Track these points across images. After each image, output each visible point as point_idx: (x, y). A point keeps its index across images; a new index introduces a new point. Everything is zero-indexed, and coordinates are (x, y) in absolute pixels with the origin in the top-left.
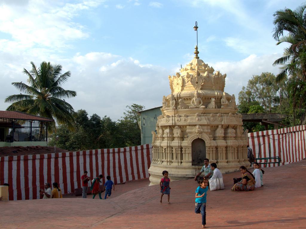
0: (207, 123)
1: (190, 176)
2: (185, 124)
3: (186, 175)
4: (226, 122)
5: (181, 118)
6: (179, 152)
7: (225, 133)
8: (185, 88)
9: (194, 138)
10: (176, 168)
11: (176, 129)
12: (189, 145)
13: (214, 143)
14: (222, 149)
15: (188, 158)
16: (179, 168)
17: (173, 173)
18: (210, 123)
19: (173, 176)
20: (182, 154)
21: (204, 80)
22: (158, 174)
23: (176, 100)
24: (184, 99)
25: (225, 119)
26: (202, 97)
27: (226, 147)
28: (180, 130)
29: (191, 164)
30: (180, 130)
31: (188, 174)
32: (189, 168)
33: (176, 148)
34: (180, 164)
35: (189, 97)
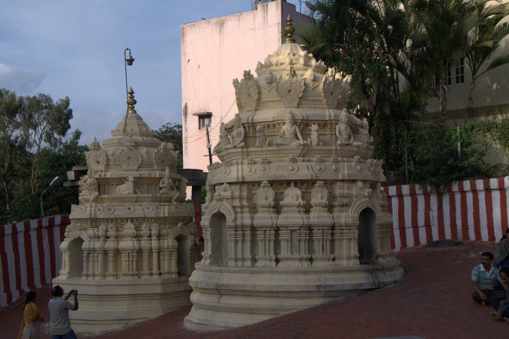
0: (312, 176)
1: (367, 287)
2: (334, 177)
3: (360, 285)
4: (346, 175)
5: (271, 165)
6: (273, 238)
7: (278, 198)
8: (304, 102)
9: (362, 207)
10: (297, 272)
11: (264, 187)
12: (356, 222)
13: (343, 217)
14: (323, 232)
15: (348, 249)
16: (305, 272)
17: (332, 283)
18: (316, 176)
19: (334, 289)
20: (332, 241)
21: (304, 87)
22: (298, 289)
23: (247, 129)
24: (268, 125)
25: (346, 167)
26: (300, 121)
27: (333, 227)
28: (327, 190)
29: (358, 261)
30: (327, 190)
31: (363, 282)
32: (358, 271)
33: (266, 230)
34: (273, 263)
35: (273, 121)
